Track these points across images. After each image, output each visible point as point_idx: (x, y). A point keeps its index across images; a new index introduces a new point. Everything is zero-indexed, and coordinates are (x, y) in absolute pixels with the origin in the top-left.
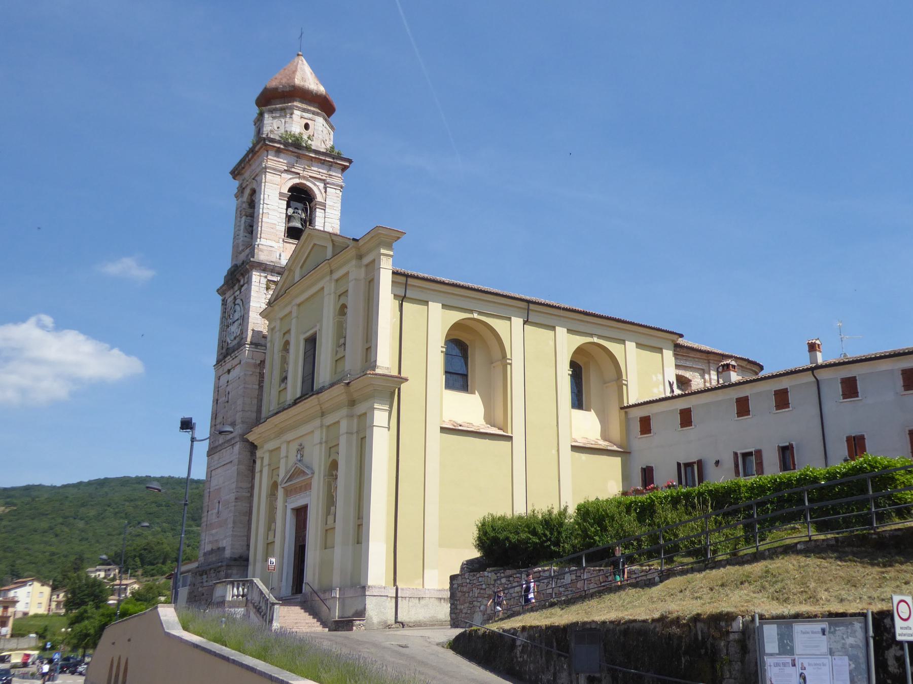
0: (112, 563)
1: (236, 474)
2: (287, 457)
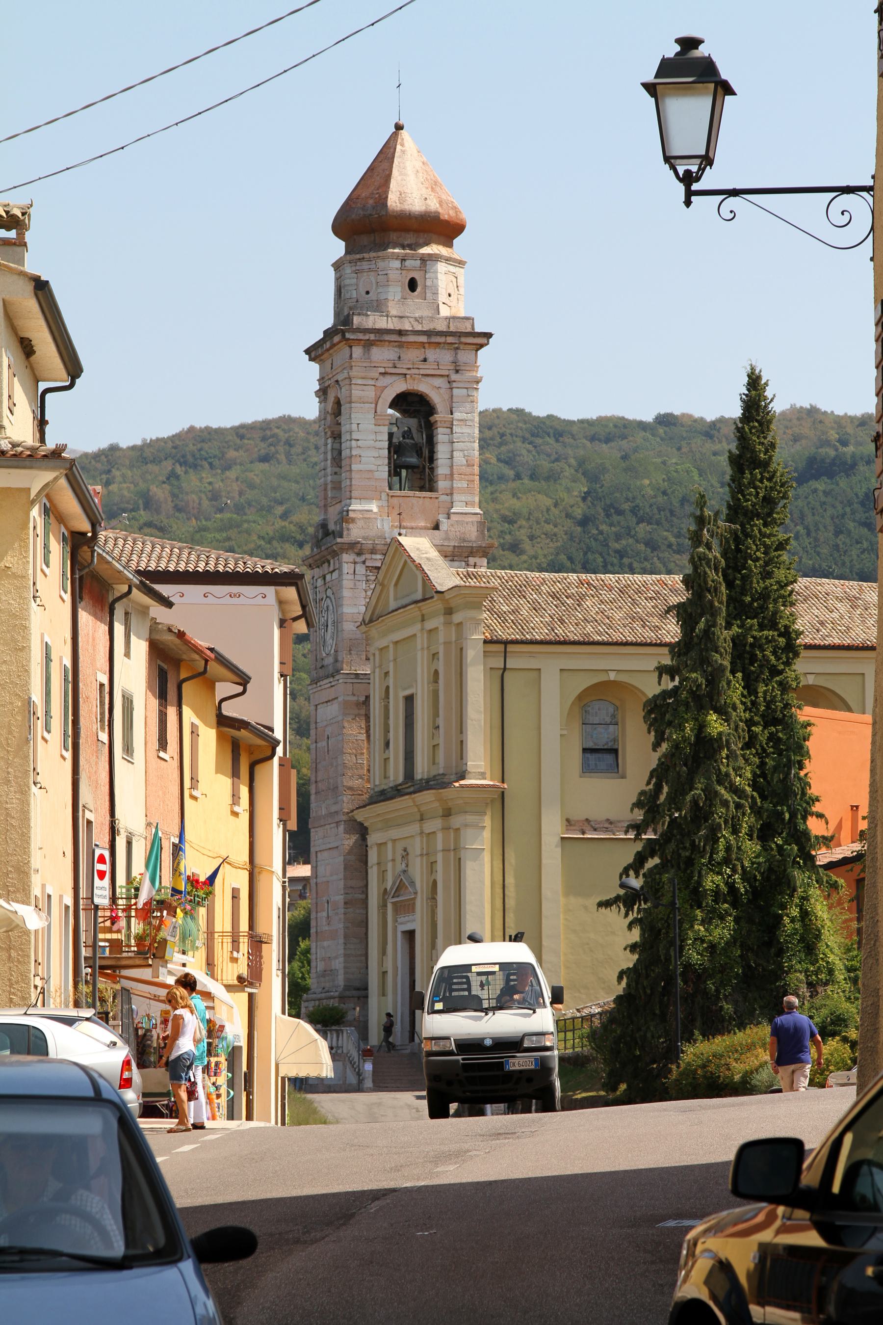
0: (552, 435)
1: (343, 866)
2: (393, 860)
